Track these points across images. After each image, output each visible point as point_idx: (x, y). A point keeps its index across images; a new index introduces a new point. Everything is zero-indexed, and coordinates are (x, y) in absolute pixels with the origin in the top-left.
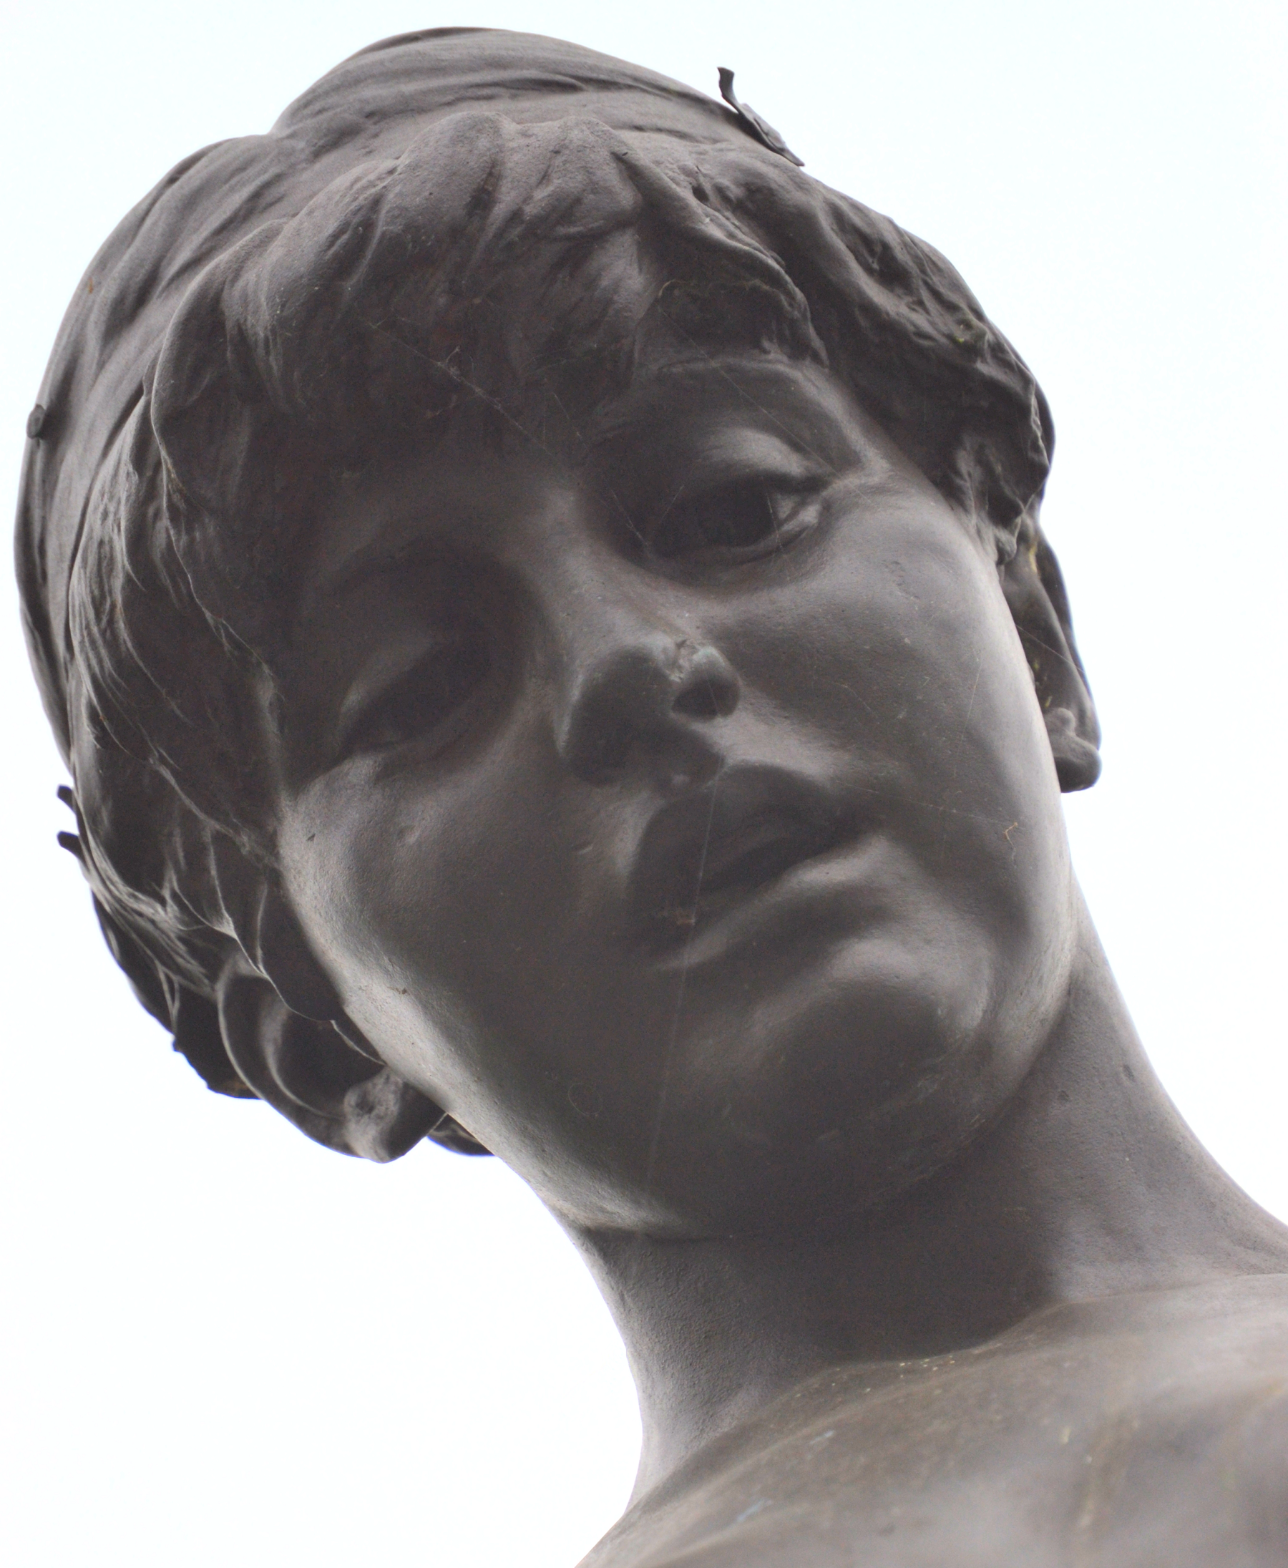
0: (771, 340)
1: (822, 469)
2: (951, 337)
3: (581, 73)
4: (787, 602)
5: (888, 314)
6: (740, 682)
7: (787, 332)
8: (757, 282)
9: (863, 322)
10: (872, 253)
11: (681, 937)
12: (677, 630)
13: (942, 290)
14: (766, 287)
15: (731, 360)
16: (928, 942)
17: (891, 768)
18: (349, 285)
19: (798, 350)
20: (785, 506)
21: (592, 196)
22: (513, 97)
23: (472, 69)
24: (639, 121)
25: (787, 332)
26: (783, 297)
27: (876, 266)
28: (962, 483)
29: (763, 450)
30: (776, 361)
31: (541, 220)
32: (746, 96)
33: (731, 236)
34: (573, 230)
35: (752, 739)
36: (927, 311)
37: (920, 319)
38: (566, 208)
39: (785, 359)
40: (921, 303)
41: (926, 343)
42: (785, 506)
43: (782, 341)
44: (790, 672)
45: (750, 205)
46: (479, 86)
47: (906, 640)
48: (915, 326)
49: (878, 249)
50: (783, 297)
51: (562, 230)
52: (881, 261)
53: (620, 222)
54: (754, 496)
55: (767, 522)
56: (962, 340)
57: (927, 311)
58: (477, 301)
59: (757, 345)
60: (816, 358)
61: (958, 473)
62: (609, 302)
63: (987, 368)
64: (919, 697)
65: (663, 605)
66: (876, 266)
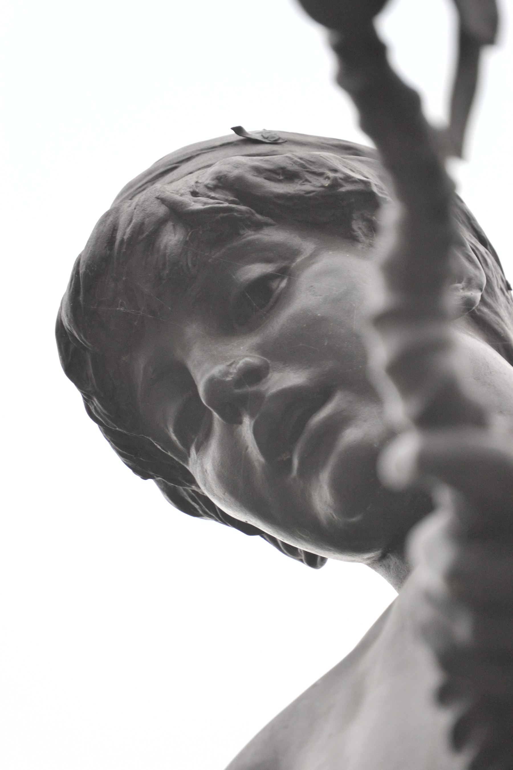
0: (244, 229)
1: (284, 264)
2: (323, 186)
3: (175, 161)
4: (281, 321)
5: (289, 193)
6: (269, 362)
7: (249, 223)
8: (221, 215)
9: (280, 202)
10: (278, 174)
11: (290, 462)
12: (242, 353)
13: (316, 170)
14: (225, 215)
15: (229, 246)
16: (365, 421)
17: (329, 365)
18: (81, 298)
19: (258, 226)
20: (274, 285)
21: (147, 219)
22: (153, 184)
23: (140, 181)
24: (190, 171)
25: (249, 223)
26: (235, 214)
27: (281, 178)
28: (355, 233)
29: (256, 270)
30: (251, 236)
31: (130, 238)
32: (252, 129)
33: (205, 204)
34: (144, 235)
35: (288, 378)
36: (310, 182)
37: (308, 187)
38: (139, 229)
39: (253, 233)
40: (307, 180)
41: (312, 194)
42: (274, 285)
43: (249, 227)
44: (284, 351)
45: (220, 185)
46: (137, 189)
47: (319, 315)
48: (304, 191)
49: (280, 171)
50: (235, 214)
51: (141, 238)
52: (283, 175)
53: (162, 222)
54: (263, 284)
55: (269, 292)
56: (327, 185)
57: (310, 182)
58: (124, 278)
59: (241, 235)
60: (267, 225)
61: (354, 231)
62: (165, 255)
63: (347, 188)
64: (330, 333)
65: (231, 350)
66: (281, 178)
